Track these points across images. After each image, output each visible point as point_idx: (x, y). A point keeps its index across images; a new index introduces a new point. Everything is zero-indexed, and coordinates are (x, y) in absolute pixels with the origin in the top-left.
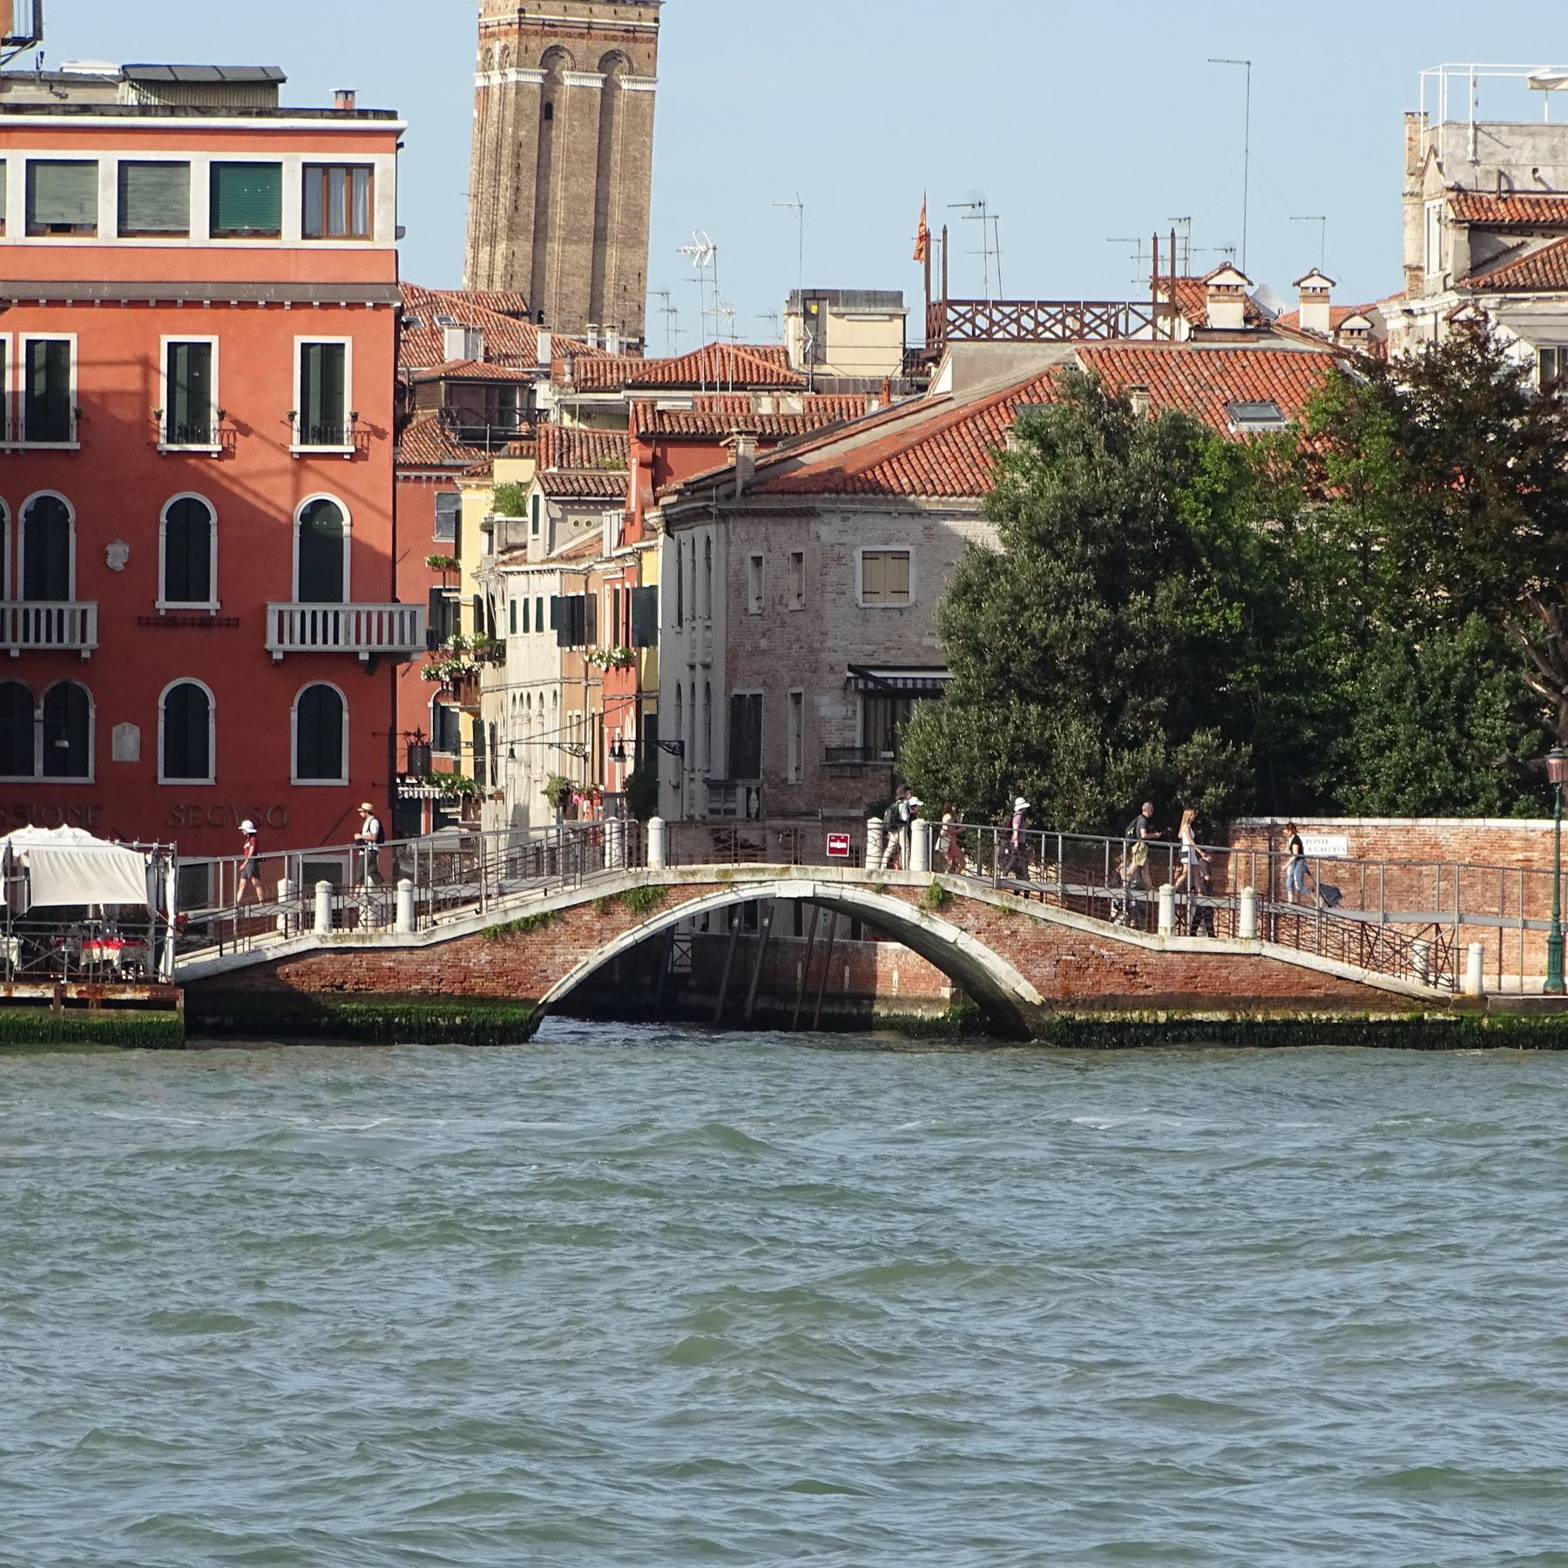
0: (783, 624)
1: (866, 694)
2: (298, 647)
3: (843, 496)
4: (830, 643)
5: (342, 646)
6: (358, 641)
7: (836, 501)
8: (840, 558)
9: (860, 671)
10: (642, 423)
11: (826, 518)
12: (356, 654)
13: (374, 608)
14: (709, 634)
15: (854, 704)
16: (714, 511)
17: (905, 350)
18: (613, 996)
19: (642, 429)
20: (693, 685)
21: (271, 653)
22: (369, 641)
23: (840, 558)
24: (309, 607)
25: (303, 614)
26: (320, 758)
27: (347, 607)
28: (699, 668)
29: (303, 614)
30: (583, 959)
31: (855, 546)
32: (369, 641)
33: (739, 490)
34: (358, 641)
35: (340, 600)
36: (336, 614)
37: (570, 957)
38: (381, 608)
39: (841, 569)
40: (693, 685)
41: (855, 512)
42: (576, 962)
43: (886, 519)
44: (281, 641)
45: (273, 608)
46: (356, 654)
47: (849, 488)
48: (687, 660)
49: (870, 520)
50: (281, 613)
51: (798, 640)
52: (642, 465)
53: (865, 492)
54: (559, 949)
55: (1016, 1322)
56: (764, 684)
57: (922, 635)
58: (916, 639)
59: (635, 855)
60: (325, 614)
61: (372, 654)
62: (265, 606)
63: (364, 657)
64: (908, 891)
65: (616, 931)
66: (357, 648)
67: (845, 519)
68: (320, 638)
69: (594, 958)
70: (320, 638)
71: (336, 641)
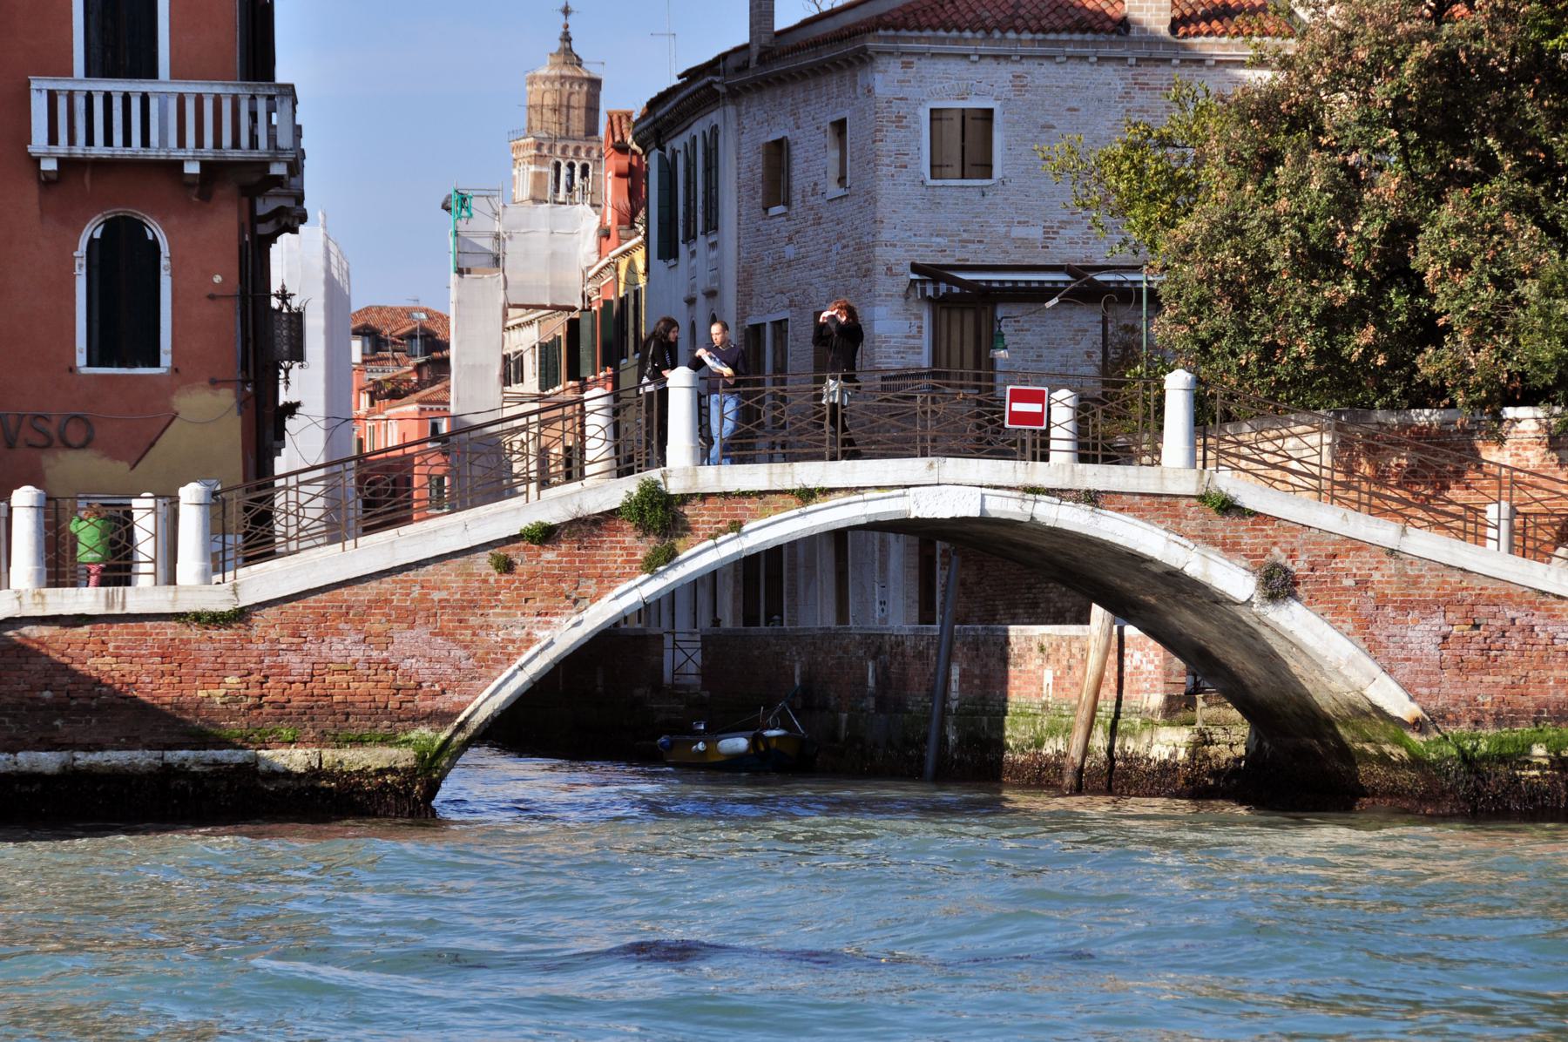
0: (818, 221)
1: (939, 304)
2: (80, 150)
3: (903, 33)
4: (885, 235)
5: (155, 152)
6: (181, 143)
7: (895, 39)
8: (900, 118)
9: (930, 273)
10: (617, 132)
11: (882, 63)
12: (179, 164)
13: (208, 89)
14: (713, 254)
15: (920, 318)
16: (721, 89)
17: (685, 499)
18: (588, 711)
19: (618, 138)
20: (693, 325)
21: (37, 161)
22: (200, 143)
23: (900, 118)
24: (101, 86)
25: (89, 98)
26: (124, 328)
27: (164, 86)
28: (701, 299)
29: (89, 98)
30: (543, 635)
31: (921, 102)
32: (200, 143)
33: (755, 58)
34: (181, 143)
35: (152, 73)
36: (145, 99)
37: (518, 633)
38: (218, 89)
39: (902, 133)
40: (693, 325)
41: (921, 55)
42: (529, 641)
43: (963, 64)
44: (53, 139)
45: (39, 90)
46: (179, 164)
47: (912, 22)
48: (684, 294)
49: (941, 65)
50: (52, 97)
51: (841, 237)
52: (619, 175)
53: (935, 29)
54: (495, 617)
55: (959, 994)
56: (792, 304)
57: (1009, 225)
58: (1002, 230)
59: (639, 443)
60: (126, 98)
61: (204, 165)
62: (29, 83)
63: (192, 168)
64: (1159, 506)
65: (606, 580)
66: (178, 154)
67: (907, 65)
68: (118, 137)
69: (565, 633)
70: (118, 137)
71: (145, 142)
